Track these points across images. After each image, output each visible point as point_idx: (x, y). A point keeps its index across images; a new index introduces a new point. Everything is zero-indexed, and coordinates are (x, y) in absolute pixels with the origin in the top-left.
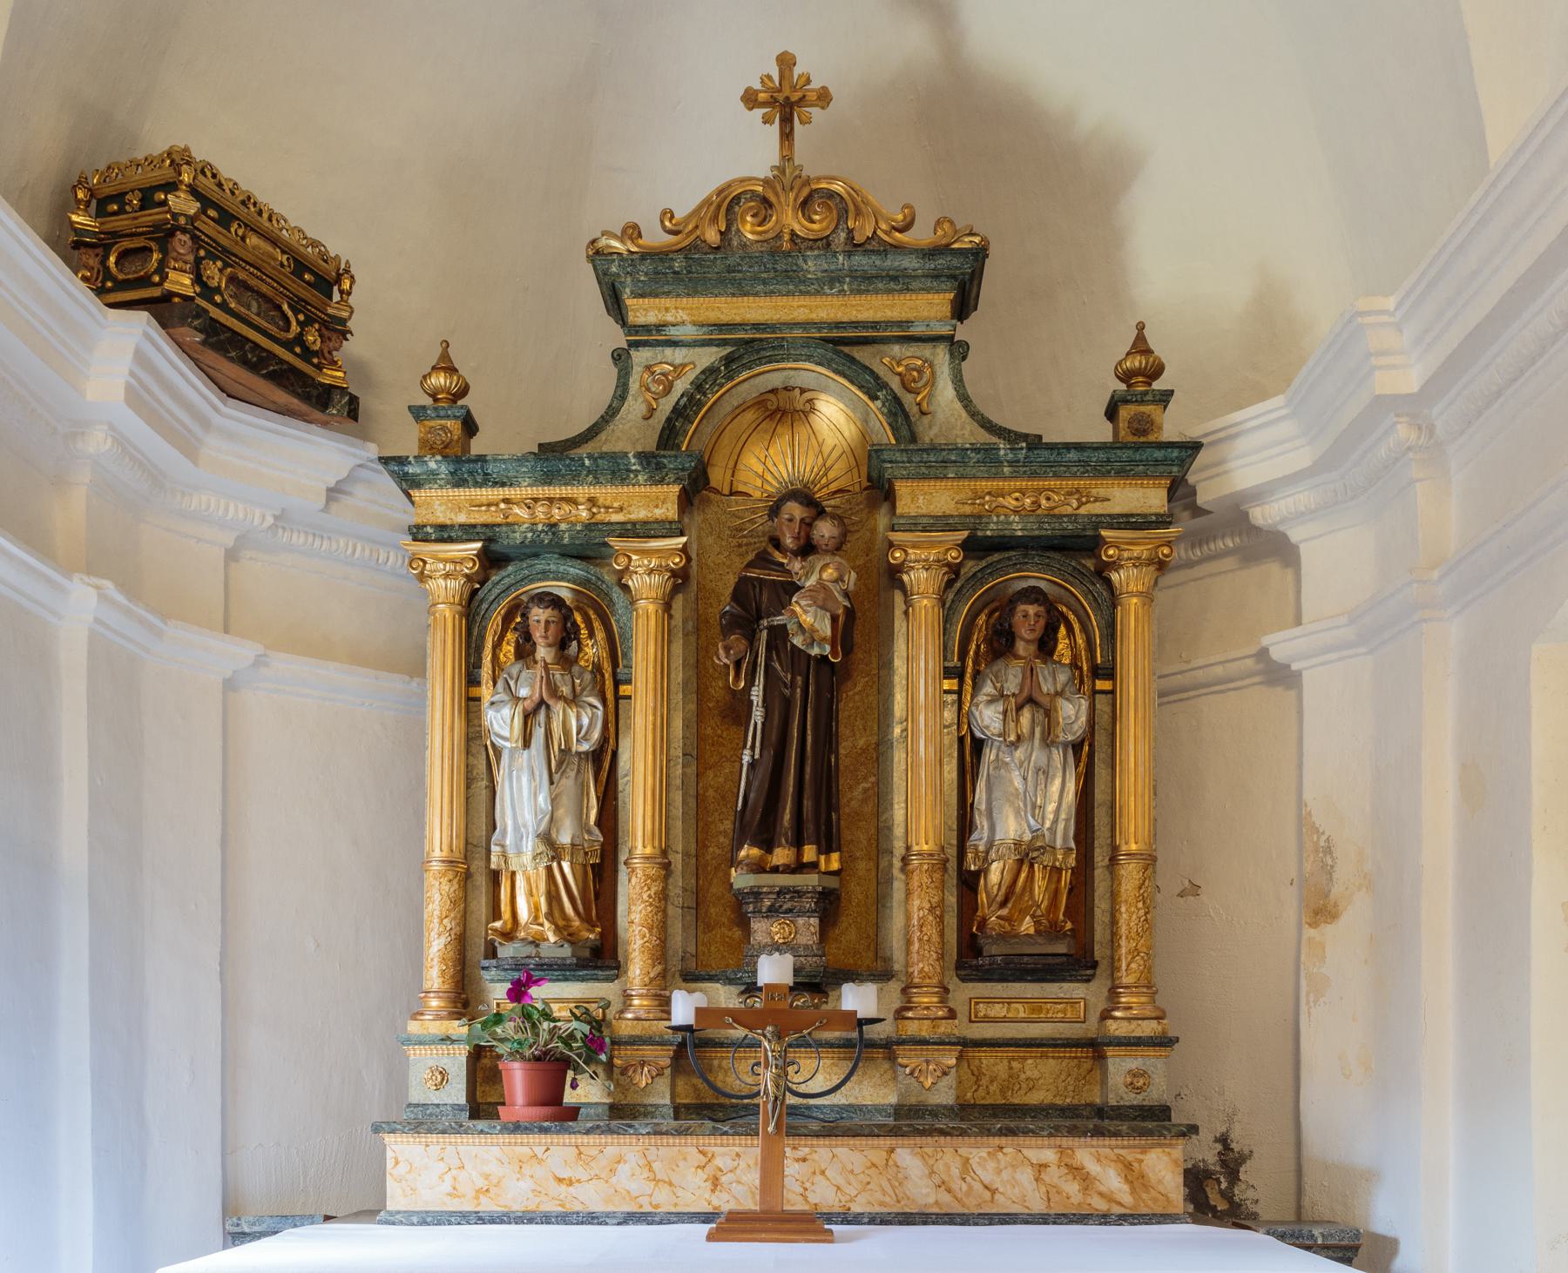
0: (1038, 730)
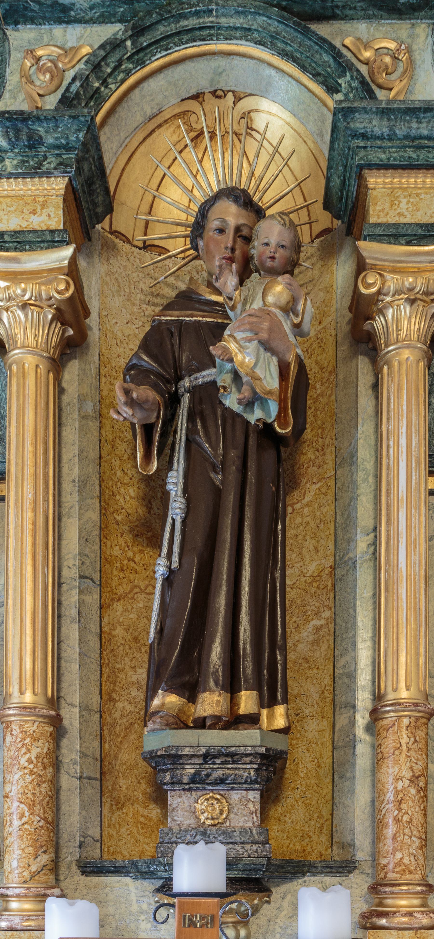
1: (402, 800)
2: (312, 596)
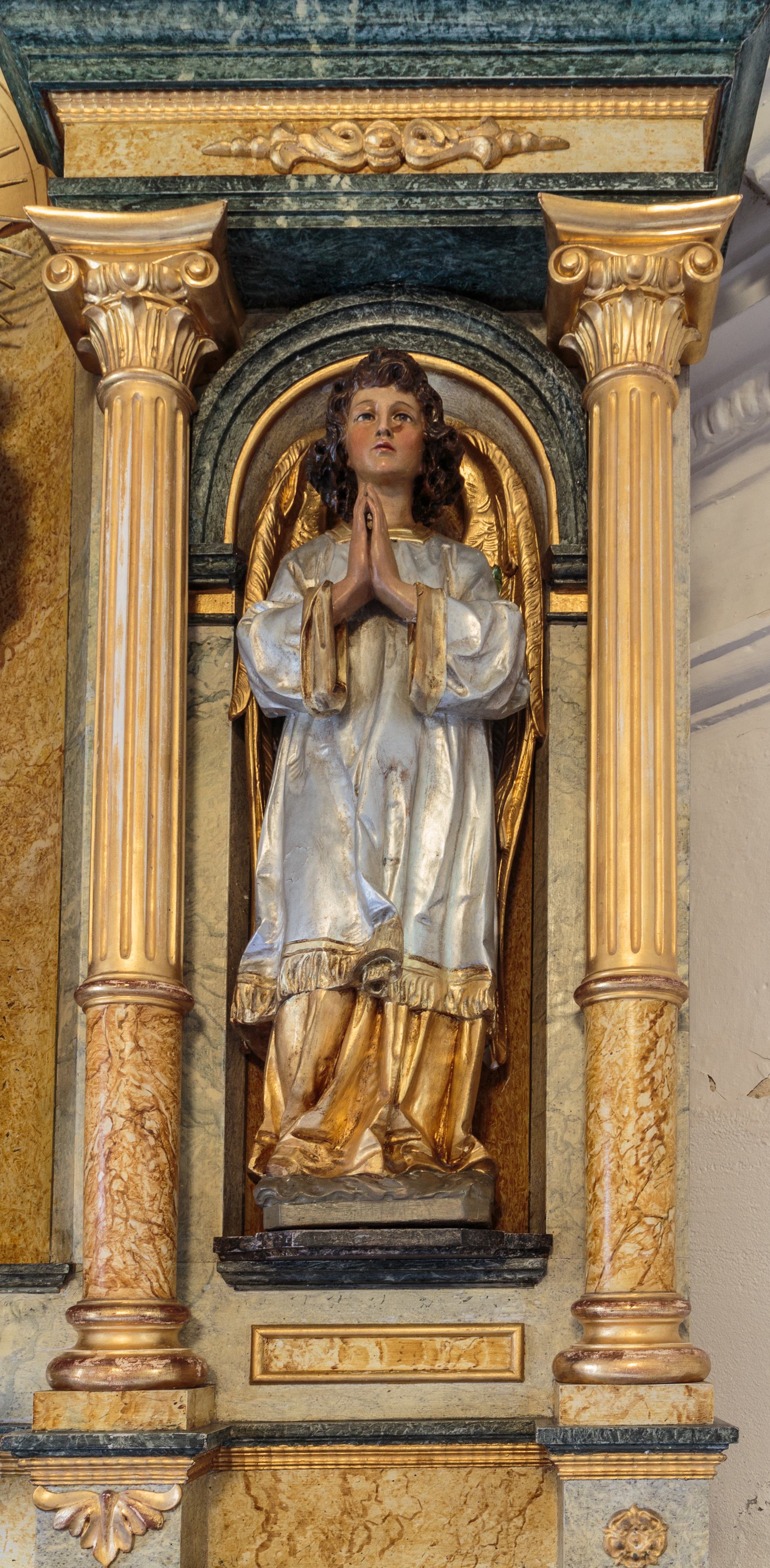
0: (392, 674)
1: (110, 1152)
2: (35, 799)
